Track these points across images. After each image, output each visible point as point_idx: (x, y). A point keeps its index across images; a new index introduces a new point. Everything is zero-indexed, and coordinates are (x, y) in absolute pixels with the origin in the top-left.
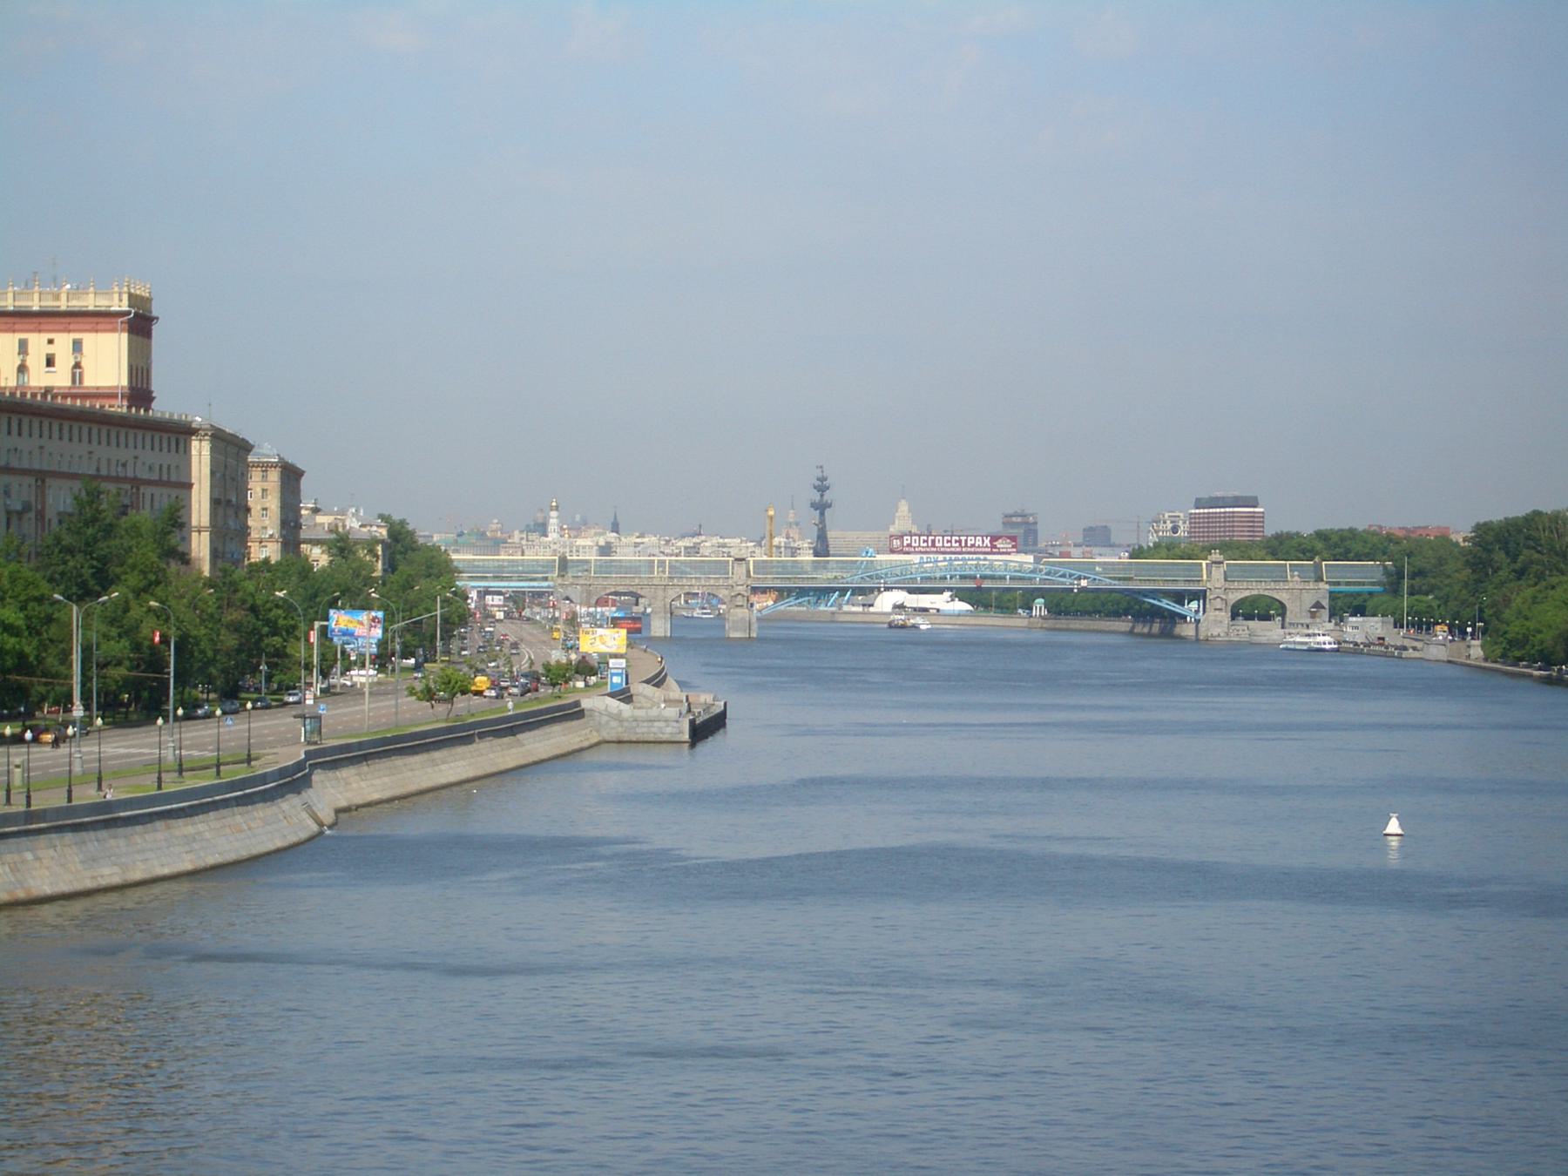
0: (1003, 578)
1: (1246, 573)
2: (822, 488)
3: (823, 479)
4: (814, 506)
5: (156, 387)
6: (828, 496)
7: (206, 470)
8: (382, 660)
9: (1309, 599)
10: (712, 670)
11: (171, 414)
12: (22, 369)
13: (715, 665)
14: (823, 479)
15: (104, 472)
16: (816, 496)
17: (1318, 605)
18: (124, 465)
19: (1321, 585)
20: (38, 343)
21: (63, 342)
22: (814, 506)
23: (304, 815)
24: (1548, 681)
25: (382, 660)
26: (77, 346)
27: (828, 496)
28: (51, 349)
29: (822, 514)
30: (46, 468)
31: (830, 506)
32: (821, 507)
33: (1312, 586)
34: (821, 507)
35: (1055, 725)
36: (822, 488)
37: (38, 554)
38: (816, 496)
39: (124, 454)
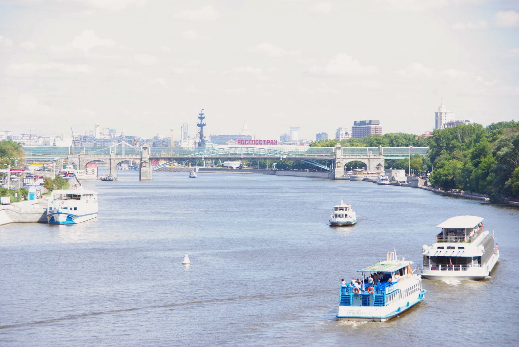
0: (252, 154)
1: (353, 153)
4: (199, 125)
5: (477, 224)
6: (204, 121)
7: (242, 177)
10: (98, 187)
12: (201, 143)
13: (106, 186)
14: (202, 114)
16: (199, 121)
17: (379, 165)
19: (382, 157)
22: (199, 125)
23: (81, 312)
24: (444, 195)
27: (204, 121)
29: (202, 129)
31: (205, 125)
33: (378, 157)
38: (199, 121)
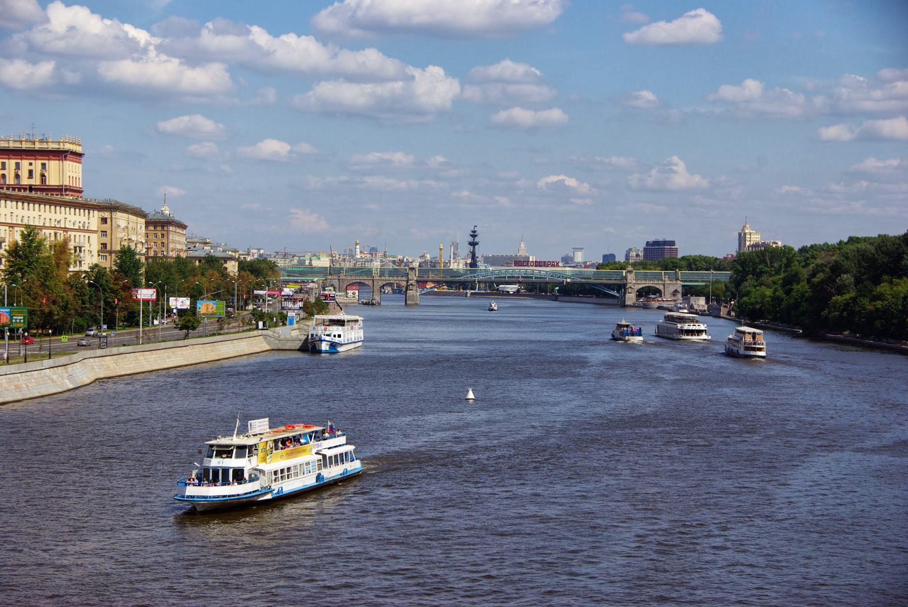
1: (645, 276)
2: (474, 235)
3: (474, 232)
4: (470, 244)
6: (476, 240)
8: (321, 340)
9: (672, 289)
11: (86, 200)
14: (474, 232)
15: (47, 224)
16: (471, 239)
17: (676, 291)
18: (59, 222)
20: (25, 164)
21: (37, 164)
22: (470, 244)
25: (321, 340)
26: (44, 165)
27: (476, 240)
28: (31, 168)
30: (14, 222)
32: (473, 244)
34: (473, 244)
35: (404, 342)
36: (474, 235)
37: (862, 255)
38: (471, 239)
39: (58, 217)
